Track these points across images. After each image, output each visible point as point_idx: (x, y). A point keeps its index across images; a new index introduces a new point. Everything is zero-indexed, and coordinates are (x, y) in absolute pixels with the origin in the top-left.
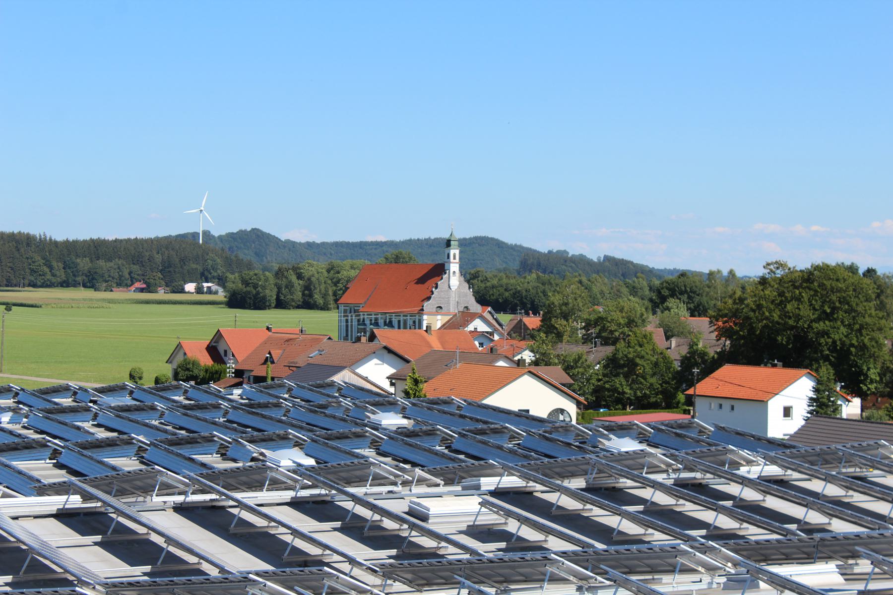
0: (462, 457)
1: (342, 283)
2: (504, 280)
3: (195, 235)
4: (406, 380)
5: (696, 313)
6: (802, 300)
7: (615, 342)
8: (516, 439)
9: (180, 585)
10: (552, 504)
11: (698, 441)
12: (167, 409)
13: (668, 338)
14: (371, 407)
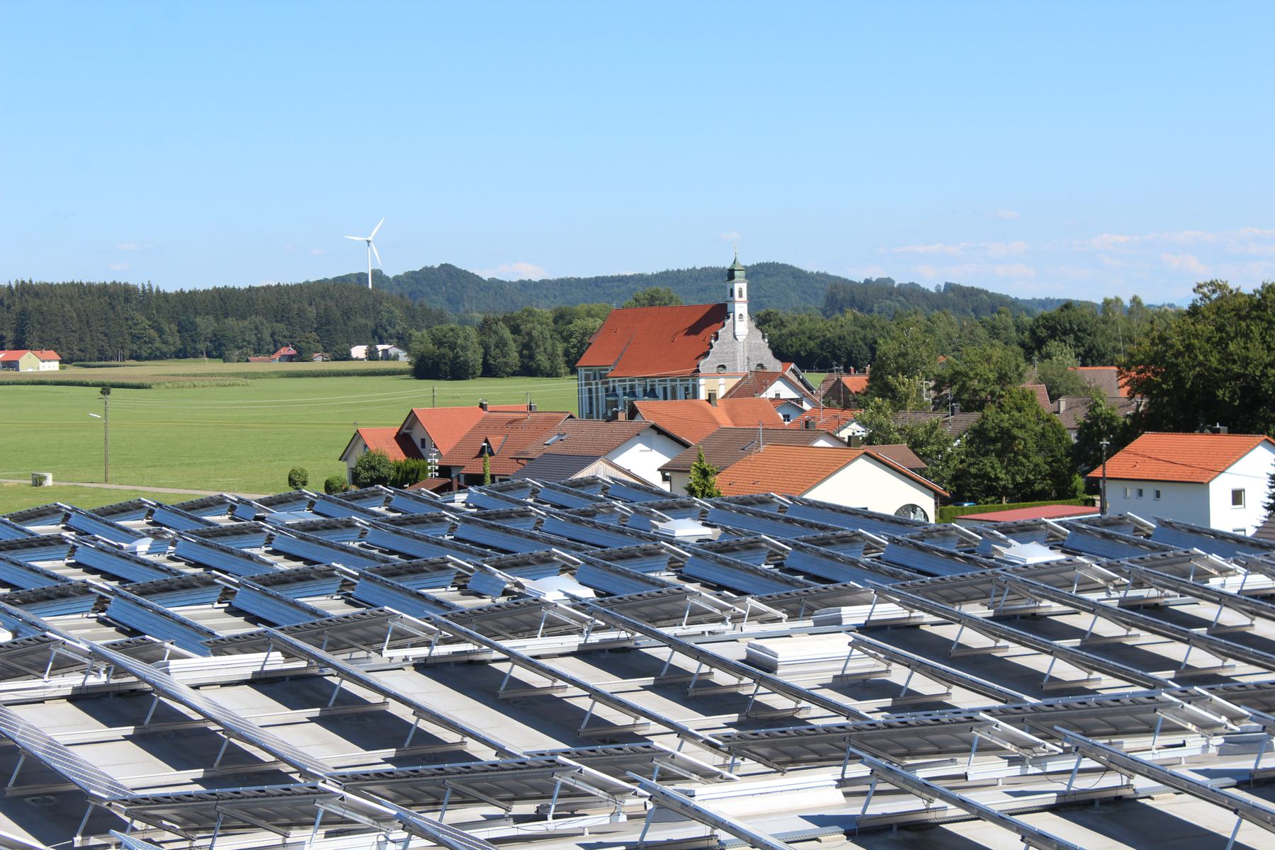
0: (801, 578)
1: (576, 338)
2: (807, 324)
3: (361, 277)
4: (688, 472)
5: (1089, 361)
6: (1251, 335)
7: (980, 406)
8: (873, 551)
9: (453, 774)
10: (950, 642)
11: (1137, 544)
12: (369, 526)
13: (1053, 398)
14: (658, 512)
